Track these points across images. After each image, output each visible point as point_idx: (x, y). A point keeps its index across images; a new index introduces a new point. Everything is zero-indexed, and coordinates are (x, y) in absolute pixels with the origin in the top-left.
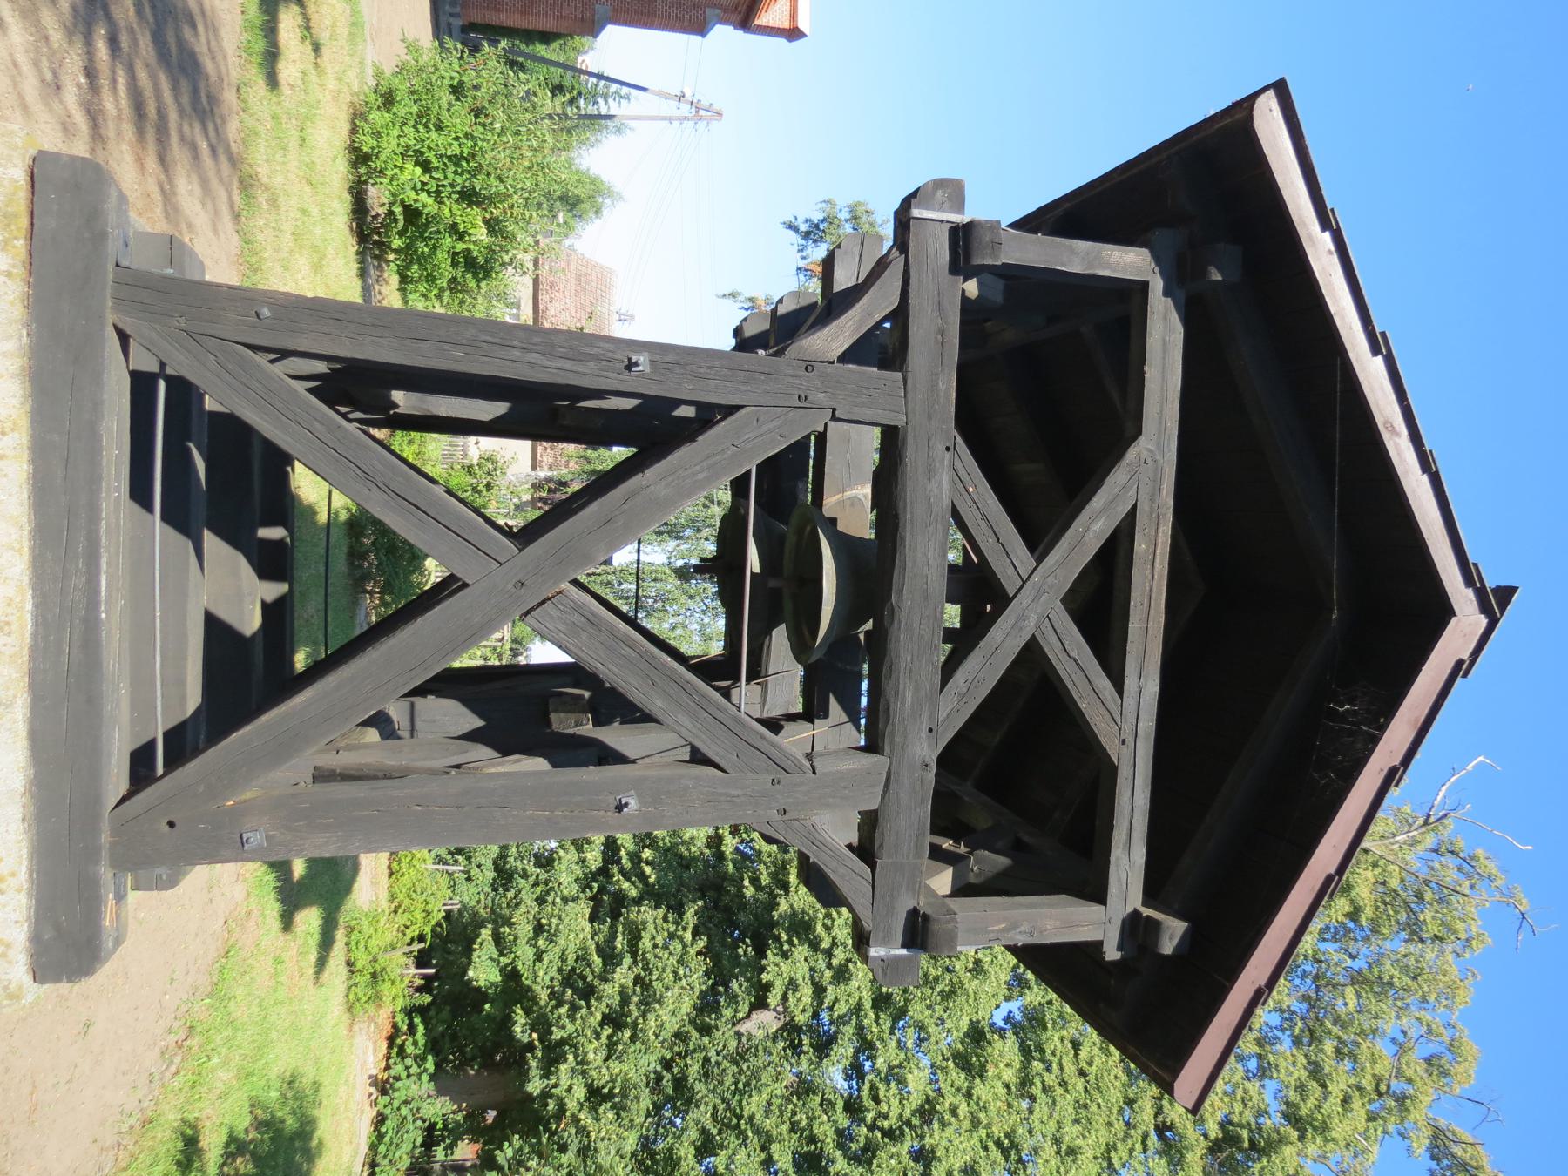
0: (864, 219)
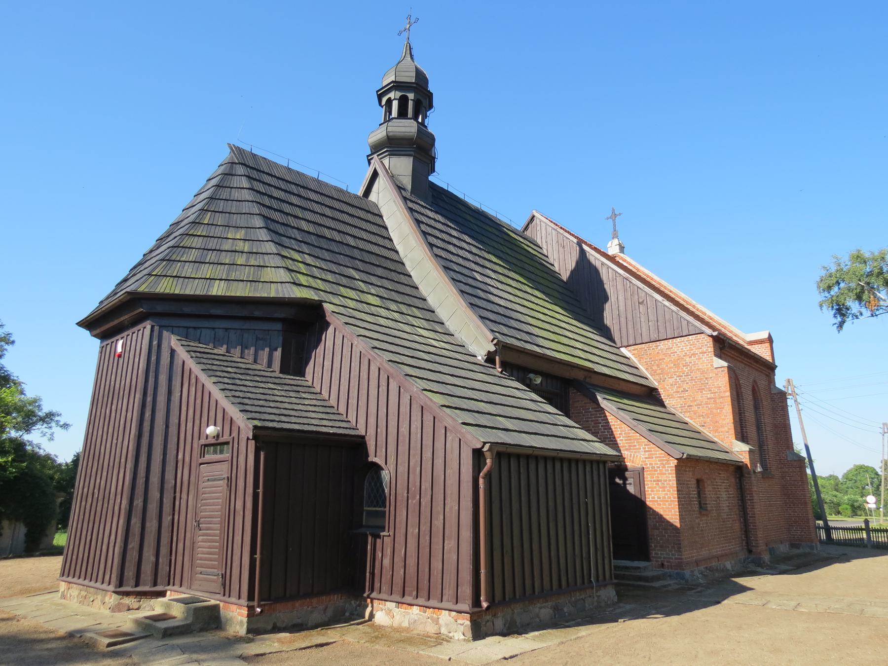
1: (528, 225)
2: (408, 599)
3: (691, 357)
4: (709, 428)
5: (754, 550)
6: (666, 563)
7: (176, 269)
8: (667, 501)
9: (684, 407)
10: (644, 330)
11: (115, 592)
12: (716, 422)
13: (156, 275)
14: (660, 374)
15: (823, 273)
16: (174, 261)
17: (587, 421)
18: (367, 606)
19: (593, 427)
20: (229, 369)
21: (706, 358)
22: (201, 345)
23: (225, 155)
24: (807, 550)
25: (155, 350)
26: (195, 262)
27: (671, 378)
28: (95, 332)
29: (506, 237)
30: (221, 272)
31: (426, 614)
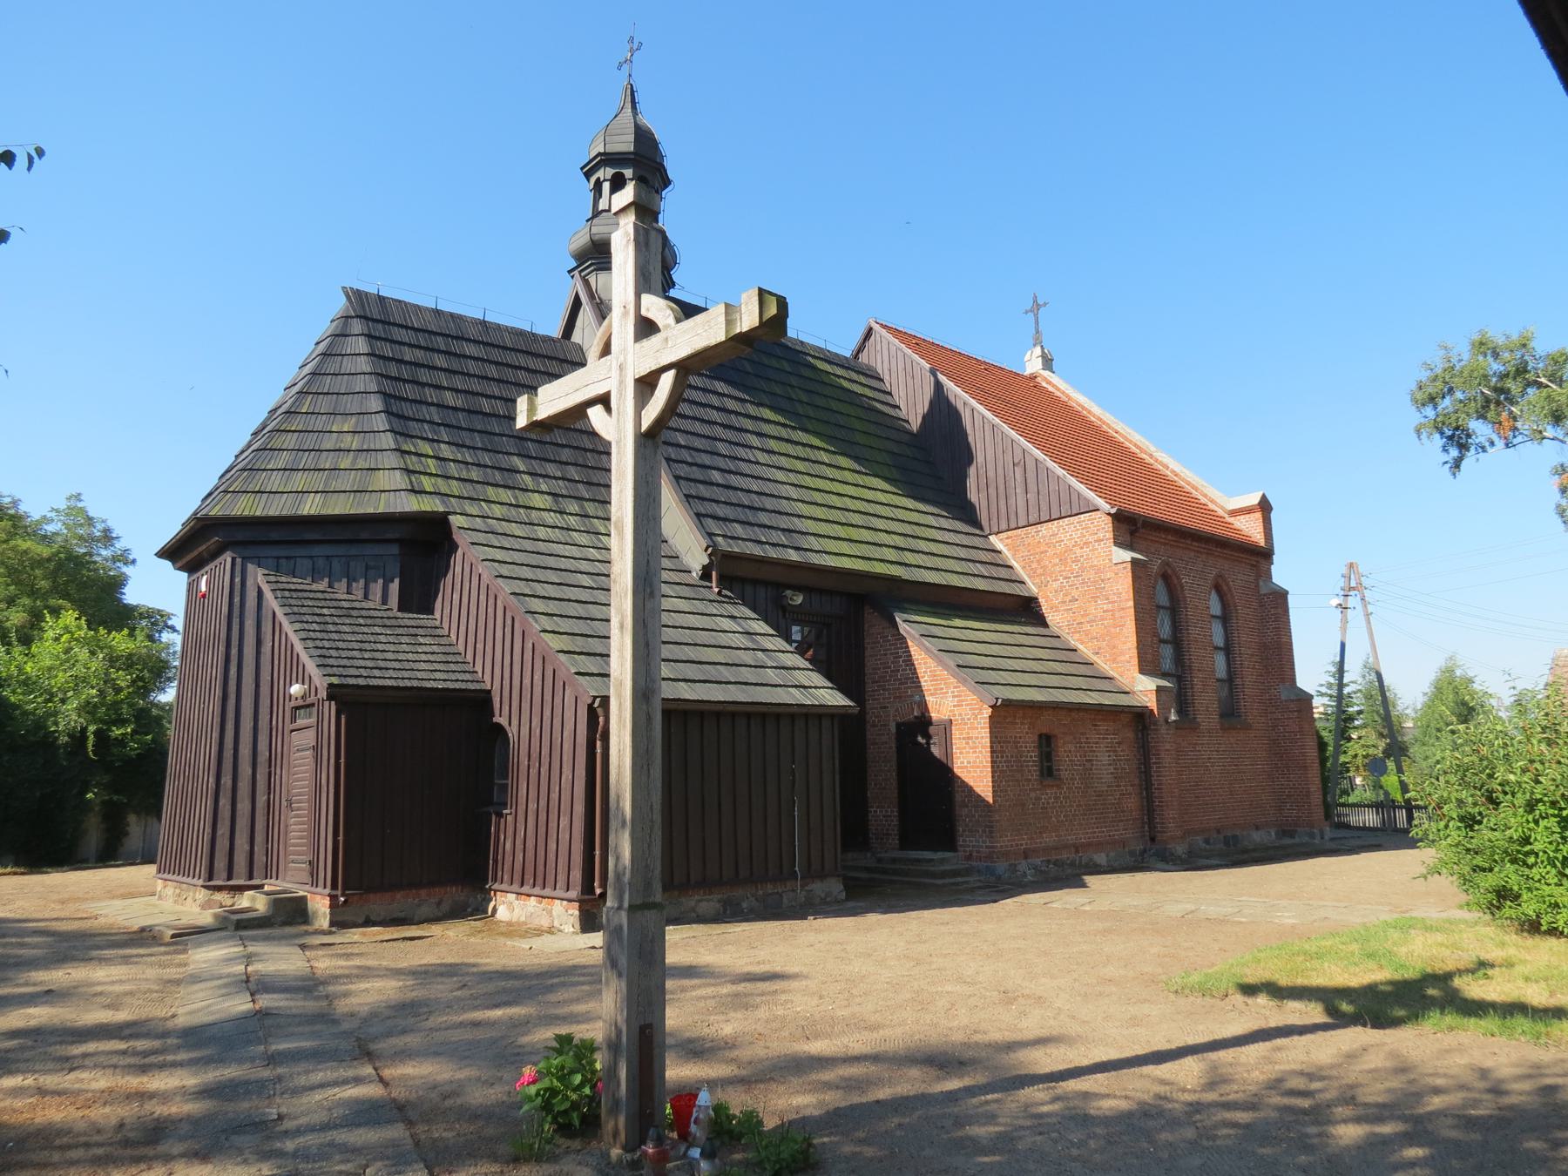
0: (1431, 390)
2: (526, 889)
3: (1082, 548)
4: (1105, 657)
7: (259, 481)
8: (978, 767)
13: (233, 492)
14: (1041, 575)
15: (1424, 375)
16: (258, 470)
17: (886, 655)
18: (491, 900)
19: (892, 663)
20: (325, 611)
22: (295, 580)
23: (339, 304)
24: (1306, 839)
25: (238, 589)
26: (285, 469)
27: (1056, 580)
28: (179, 564)
29: (807, 373)
30: (318, 480)
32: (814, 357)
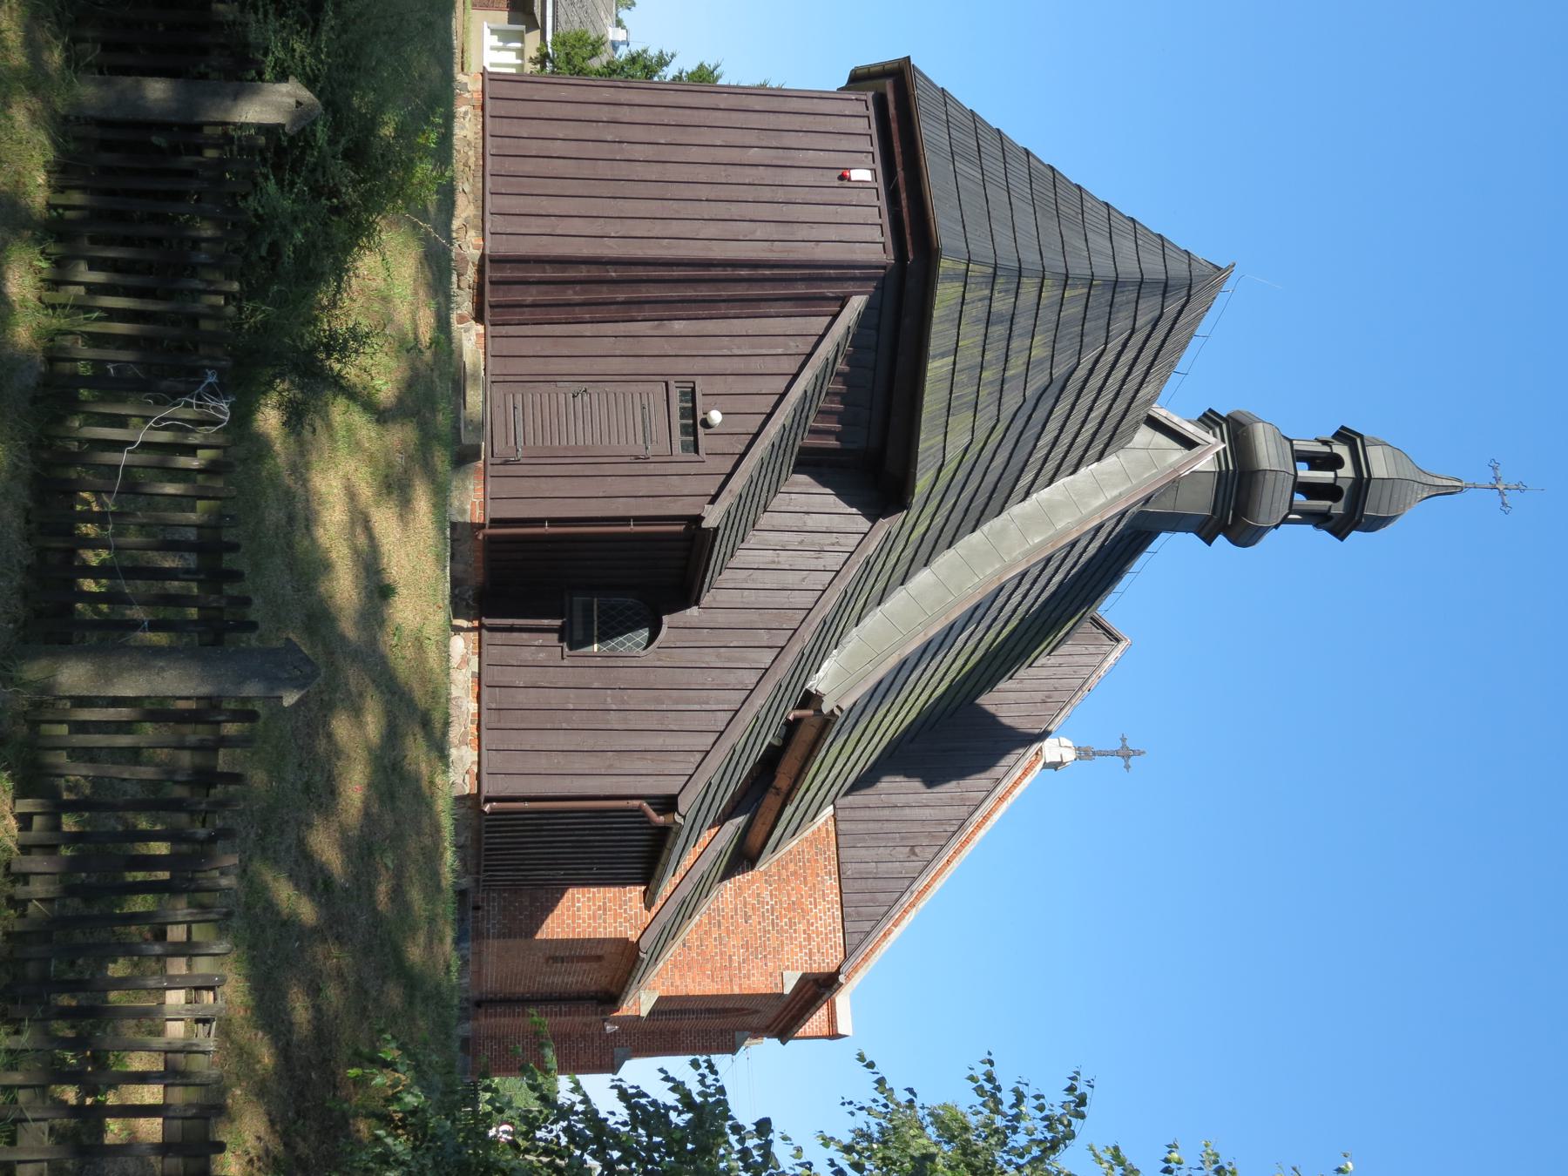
1: (1103, 628)
3: (804, 932)
4: (680, 954)
5: (480, 1011)
6: (480, 913)
8: (574, 922)
9: (719, 915)
10: (863, 852)
11: (483, 256)
12: (690, 968)
21: (801, 959)
27: (771, 895)
31: (470, 725)
32: (1084, 613)
